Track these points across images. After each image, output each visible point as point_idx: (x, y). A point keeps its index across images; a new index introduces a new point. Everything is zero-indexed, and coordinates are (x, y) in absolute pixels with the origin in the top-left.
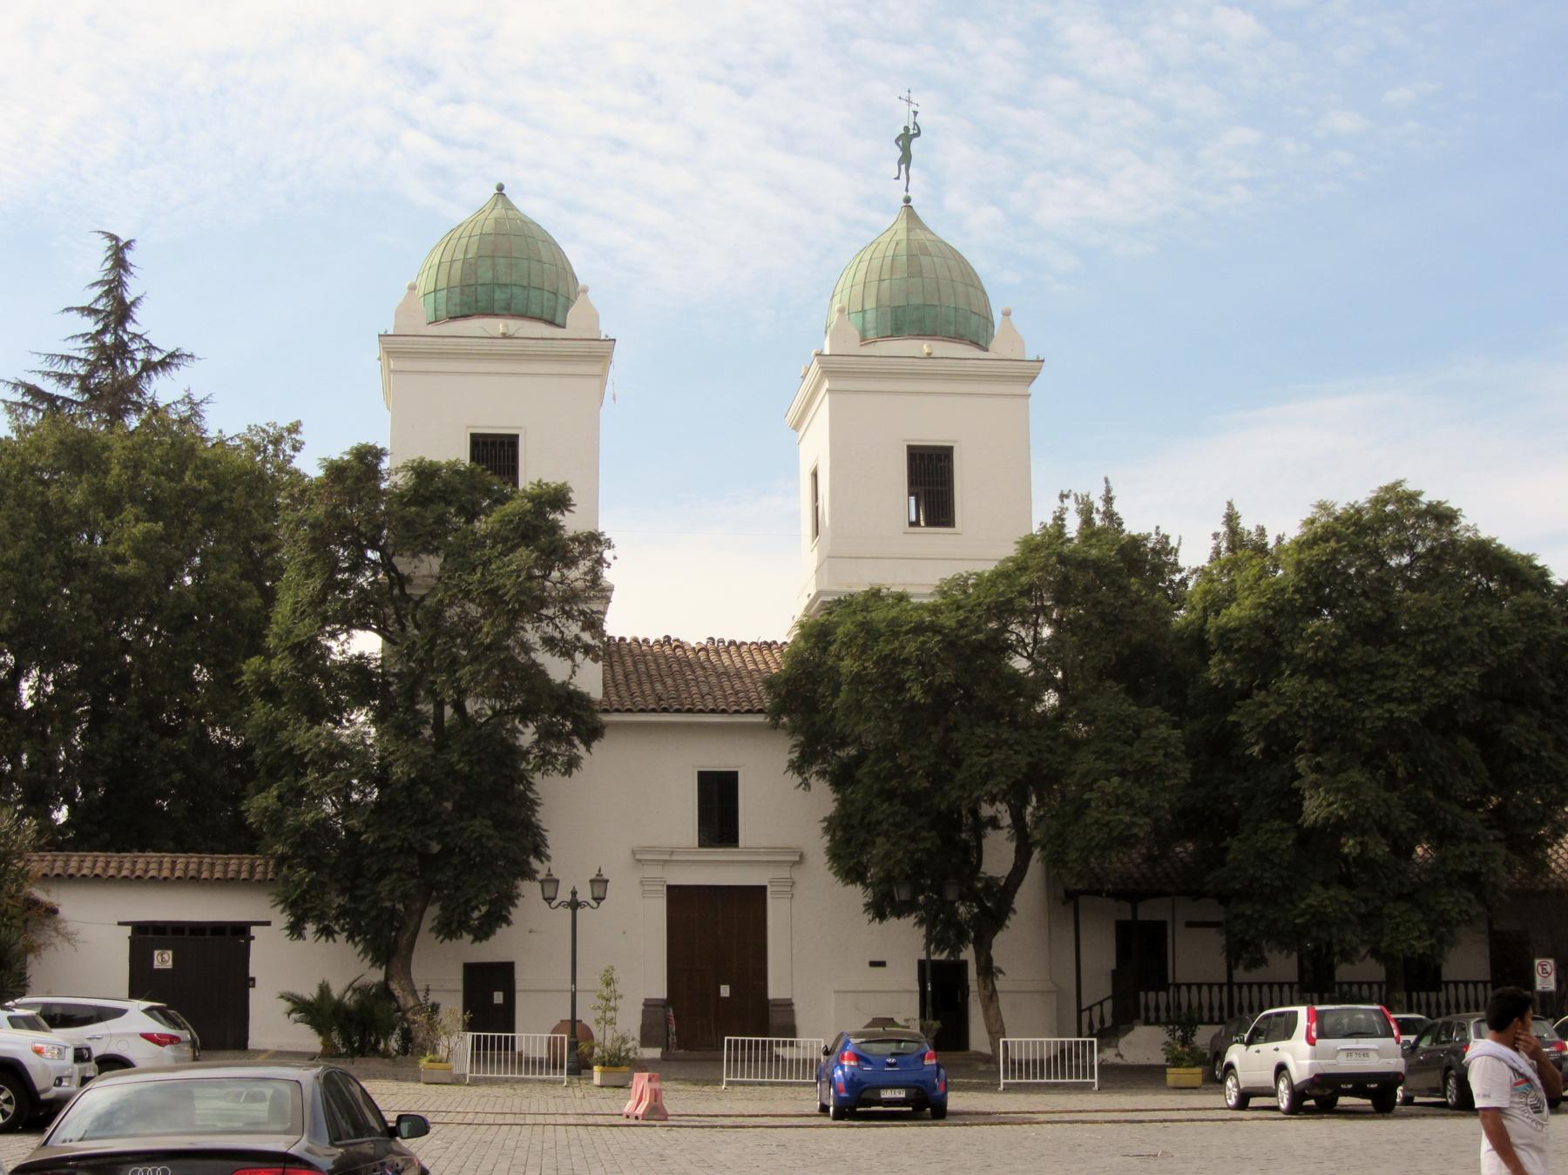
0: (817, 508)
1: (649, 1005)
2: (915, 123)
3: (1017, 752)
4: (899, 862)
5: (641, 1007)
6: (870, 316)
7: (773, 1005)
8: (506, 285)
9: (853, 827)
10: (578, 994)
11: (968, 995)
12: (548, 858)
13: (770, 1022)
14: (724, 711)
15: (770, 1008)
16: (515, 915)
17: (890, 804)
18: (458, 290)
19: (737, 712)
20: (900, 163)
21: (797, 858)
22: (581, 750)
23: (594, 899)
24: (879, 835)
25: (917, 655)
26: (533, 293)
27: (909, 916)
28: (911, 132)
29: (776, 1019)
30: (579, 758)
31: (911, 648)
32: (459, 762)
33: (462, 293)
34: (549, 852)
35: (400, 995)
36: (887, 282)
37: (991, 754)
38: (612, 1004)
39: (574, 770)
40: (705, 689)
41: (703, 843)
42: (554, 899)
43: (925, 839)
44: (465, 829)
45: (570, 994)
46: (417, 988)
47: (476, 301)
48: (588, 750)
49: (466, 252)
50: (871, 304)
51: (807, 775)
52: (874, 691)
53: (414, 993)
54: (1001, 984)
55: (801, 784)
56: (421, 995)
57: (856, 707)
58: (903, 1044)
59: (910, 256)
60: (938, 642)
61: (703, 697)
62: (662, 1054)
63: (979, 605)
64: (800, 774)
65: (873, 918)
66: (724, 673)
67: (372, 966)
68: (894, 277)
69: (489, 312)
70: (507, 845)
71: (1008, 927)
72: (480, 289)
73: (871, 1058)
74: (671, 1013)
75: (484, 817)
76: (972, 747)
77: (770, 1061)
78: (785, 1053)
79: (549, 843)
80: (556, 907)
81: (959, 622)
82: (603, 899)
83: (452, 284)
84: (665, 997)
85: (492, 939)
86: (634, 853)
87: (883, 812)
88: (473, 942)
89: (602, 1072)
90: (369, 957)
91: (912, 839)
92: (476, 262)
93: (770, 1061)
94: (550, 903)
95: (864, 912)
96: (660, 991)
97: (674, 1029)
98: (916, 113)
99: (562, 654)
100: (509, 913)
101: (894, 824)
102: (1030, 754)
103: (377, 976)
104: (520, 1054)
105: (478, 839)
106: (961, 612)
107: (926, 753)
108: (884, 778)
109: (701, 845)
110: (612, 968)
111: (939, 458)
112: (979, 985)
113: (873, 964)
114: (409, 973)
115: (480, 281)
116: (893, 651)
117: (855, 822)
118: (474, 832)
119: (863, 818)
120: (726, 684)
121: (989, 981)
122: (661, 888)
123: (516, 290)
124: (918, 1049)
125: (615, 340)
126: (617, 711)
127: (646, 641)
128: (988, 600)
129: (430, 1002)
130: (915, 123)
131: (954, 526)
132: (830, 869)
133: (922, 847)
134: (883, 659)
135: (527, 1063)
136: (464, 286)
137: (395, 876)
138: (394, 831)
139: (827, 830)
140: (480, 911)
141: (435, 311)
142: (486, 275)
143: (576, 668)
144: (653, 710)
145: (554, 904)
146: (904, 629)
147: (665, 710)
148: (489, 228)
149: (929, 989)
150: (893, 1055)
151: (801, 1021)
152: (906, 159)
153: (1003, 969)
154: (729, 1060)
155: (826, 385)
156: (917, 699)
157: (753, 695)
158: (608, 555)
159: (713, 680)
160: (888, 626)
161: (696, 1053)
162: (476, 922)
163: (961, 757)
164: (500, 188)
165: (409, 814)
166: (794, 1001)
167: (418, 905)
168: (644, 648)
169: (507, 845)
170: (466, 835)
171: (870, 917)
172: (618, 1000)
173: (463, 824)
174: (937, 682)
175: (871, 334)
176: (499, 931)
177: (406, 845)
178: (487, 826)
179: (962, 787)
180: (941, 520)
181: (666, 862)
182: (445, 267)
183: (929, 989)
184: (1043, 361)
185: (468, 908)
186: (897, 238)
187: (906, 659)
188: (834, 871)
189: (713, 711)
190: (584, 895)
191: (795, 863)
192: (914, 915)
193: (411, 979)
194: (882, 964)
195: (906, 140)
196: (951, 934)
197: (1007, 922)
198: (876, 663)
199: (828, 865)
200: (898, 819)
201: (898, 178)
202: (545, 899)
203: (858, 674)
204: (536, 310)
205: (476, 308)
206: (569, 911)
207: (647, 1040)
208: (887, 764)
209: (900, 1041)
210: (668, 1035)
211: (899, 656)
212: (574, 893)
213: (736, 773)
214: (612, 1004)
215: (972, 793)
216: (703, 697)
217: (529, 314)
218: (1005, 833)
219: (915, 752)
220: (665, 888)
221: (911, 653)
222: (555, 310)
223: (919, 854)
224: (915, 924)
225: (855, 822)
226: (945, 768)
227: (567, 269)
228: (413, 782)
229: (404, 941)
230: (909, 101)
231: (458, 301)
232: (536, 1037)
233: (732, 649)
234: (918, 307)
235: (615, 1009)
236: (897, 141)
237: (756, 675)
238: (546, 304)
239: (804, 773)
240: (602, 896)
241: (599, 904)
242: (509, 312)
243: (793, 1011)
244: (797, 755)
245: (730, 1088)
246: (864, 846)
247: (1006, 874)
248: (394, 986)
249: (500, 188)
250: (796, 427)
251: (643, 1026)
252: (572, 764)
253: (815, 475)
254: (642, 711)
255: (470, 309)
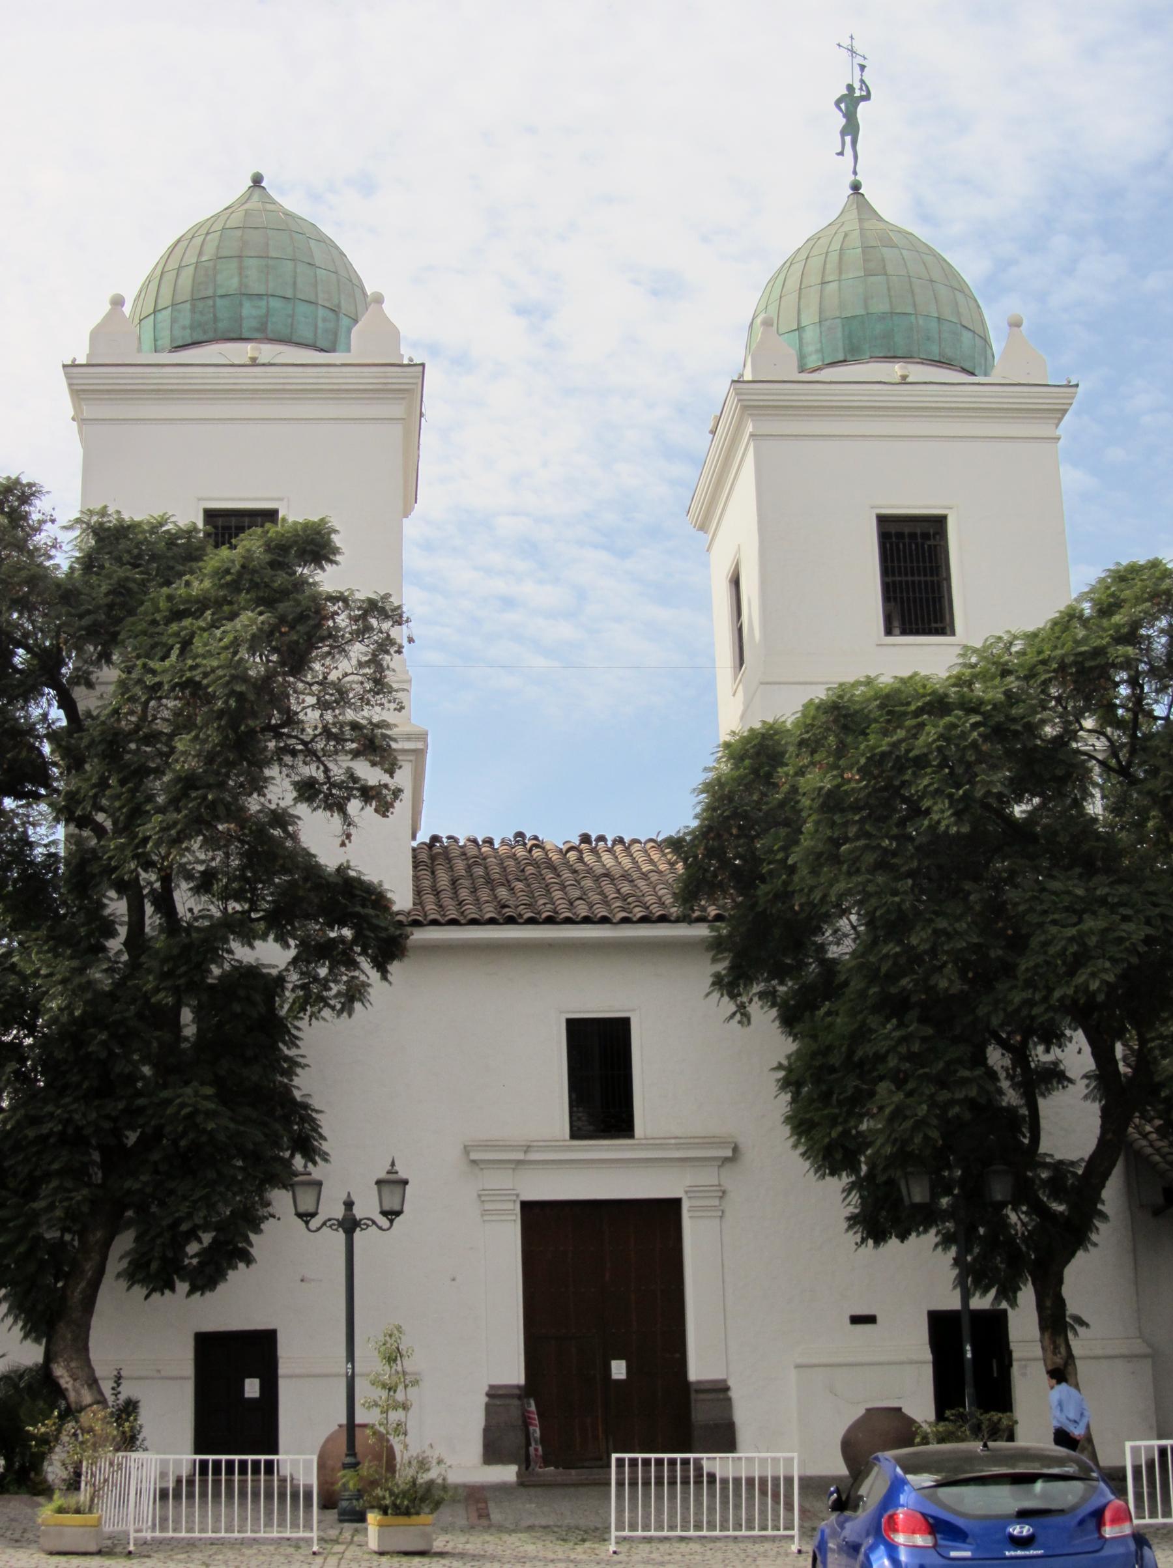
0: (740, 630)
1: (496, 1395)
2: (862, 81)
3: (1126, 919)
4: (920, 1124)
5: (484, 1399)
6: (811, 334)
7: (697, 1391)
8: (259, 296)
9: (832, 1070)
10: (357, 1380)
11: (1010, 1365)
12: (325, 1157)
13: (693, 1416)
14: (605, 920)
15: (693, 1396)
16: (259, 1244)
17: (901, 1025)
18: (188, 306)
19: (625, 920)
20: (843, 133)
21: (729, 1153)
22: (367, 970)
23: (384, 1213)
24: (881, 1078)
25: (939, 749)
26: (302, 308)
27: (926, 1231)
28: (857, 93)
29: (701, 1414)
30: (366, 985)
31: (931, 732)
32: (157, 990)
33: (193, 310)
34: (325, 1146)
35: (69, 1386)
36: (833, 286)
37: (1080, 921)
38: (400, 1396)
39: (357, 1005)
40: (575, 893)
41: (576, 1133)
42: (313, 1215)
43: (964, 1082)
44: (169, 1102)
45: (344, 1380)
46: (98, 1374)
47: (216, 319)
48: (384, 977)
49: (200, 254)
50: (810, 317)
51: (745, 999)
52: (862, 821)
53: (93, 1383)
54: (1080, 1343)
55: (734, 1014)
56: (106, 1387)
57: (829, 856)
58: (1039, 1486)
59: (866, 248)
60: (975, 726)
61: (571, 904)
62: (519, 1475)
63: (1044, 662)
64: (733, 997)
65: (863, 1240)
66: (606, 875)
67: (25, 1337)
68: (844, 277)
69: (232, 335)
70: (242, 1128)
71: (1095, 1245)
72: (219, 302)
73: (960, 1522)
74: (533, 1408)
75: (202, 1084)
76: (1045, 912)
77: (698, 1482)
78: (715, 1463)
79: (324, 1131)
80: (318, 1229)
81: (1008, 694)
82: (398, 1213)
83: (179, 299)
84: (521, 1381)
85: (221, 1288)
86: (467, 1150)
87: (887, 1037)
88: (191, 1293)
89: (381, 1525)
90: (20, 1324)
91: (942, 1082)
92: (215, 266)
93: (698, 1482)
94: (307, 1223)
95: (847, 1230)
96: (514, 1373)
97: (538, 1434)
98: (862, 67)
99: (329, 807)
100: (251, 1244)
101: (910, 1057)
102: (1148, 922)
103: (31, 1354)
104: (283, 1481)
105: (191, 1116)
106: (1011, 678)
107: (962, 926)
108: (887, 975)
109: (576, 1134)
110: (399, 1328)
111: (926, 536)
112: (1043, 1348)
113: (856, 1320)
114: (86, 1349)
115: (220, 292)
116: (895, 745)
117: (835, 1060)
118: (183, 1105)
119: (851, 1053)
120: (609, 890)
121: (1060, 1341)
122: (510, 1206)
123: (275, 303)
124: (1084, 1499)
125: (423, 365)
126: (435, 923)
127: (489, 841)
128: (1059, 652)
129: (122, 1397)
130: (862, 81)
131: (953, 633)
132: (795, 1146)
133: (959, 1095)
134: (878, 760)
135: (295, 1496)
136: (195, 300)
137: (54, 1183)
138: (50, 1108)
139: (785, 1084)
140: (200, 1241)
141: (155, 340)
142: (230, 281)
143: (352, 830)
144: (492, 921)
145: (315, 1223)
146: (913, 707)
147: (511, 921)
148: (236, 219)
149: (969, 1355)
150: (1024, 1515)
151: (743, 1415)
152: (851, 128)
153: (1085, 1318)
154: (620, 1484)
155: (750, 428)
156: (942, 828)
157: (650, 899)
158: (399, 634)
159: (588, 883)
160: (881, 707)
161: (573, 1472)
162: (195, 1261)
163: (1024, 931)
164: (257, 180)
165: (75, 1079)
166: (730, 1383)
167: (99, 1234)
168: (484, 850)
169: (242, 1128)
170: (170, 1111)
171: (858, 1238)
172: (409, 1389)
173: (165, 1094)
174: (979, 793)
175: (813, 361)
176: (231, 1274)
177: (70, 1131)
178: (206, 1098)
179: (1029, 984)
180: (933, 625)
181: (519, 1162)
182: (170, 277)
183: (969, 1355)
184: (1077, 386)
185: (179, 1242)
186: (846, 228)
187: (917, 757)
188: (801, 1149)
189: (587, 920)
190: (367, 1207)
191: (726, 1160)
192: (933, 1231)
193: (88, 1361)
194: (870, 1319)
195: (850, 102)
196: (999, 1262)
197: (1094, 1237)
198: (864, 771)
199: (793, 1140)
200: (916, 1047)
201: (841, 154)
202: (300, 1215)
203: (830, 793)
204: (306, 334)
205: (215, 331)
206: (341, 1236)
207: (493, 1453)
208: (892, 948)
209: (1030, 1479)
210: (528, 1444)
211: (908, 751)
212: (349, 1205)
213: (625, 1022)
214: (400, 1396)
215: (1050, 990)
216: (571, 904)
217: (295, 339)
218: (1080, 1088)
219: (942, 923)
220: (518, 1207)
221: (929, 745)
222: (336, 334)
223: (957, 1109)
224: (936, 1246)
225: (835, 1060)
226: (996, 953)
227: (355, 281)
228: (81, 1023)
229: (77, 1295)
230: (852, 51)
231: (187, 322)
232: (258, 1462)
233: (618, 848)
234: (883, 317)
235: (405, 1407)
236: (838, 103)
237: (654, 877)
238: (320, 324)
239: (740, 995)
240: (397, 1208)
241: (391, 1221)
242: (264, 334)
243: (729, 1400)
244: (726, 964)
245: (624, 1548)
246: (857, 1103)
247: (1087, 1157)
248: (60, 1371)
249: (257, 180)
250: (703, 527)
251: (487, 1431)
252: (354, 995)
253: (736, 582)
254: (474, 922)
255: (205, 332)
